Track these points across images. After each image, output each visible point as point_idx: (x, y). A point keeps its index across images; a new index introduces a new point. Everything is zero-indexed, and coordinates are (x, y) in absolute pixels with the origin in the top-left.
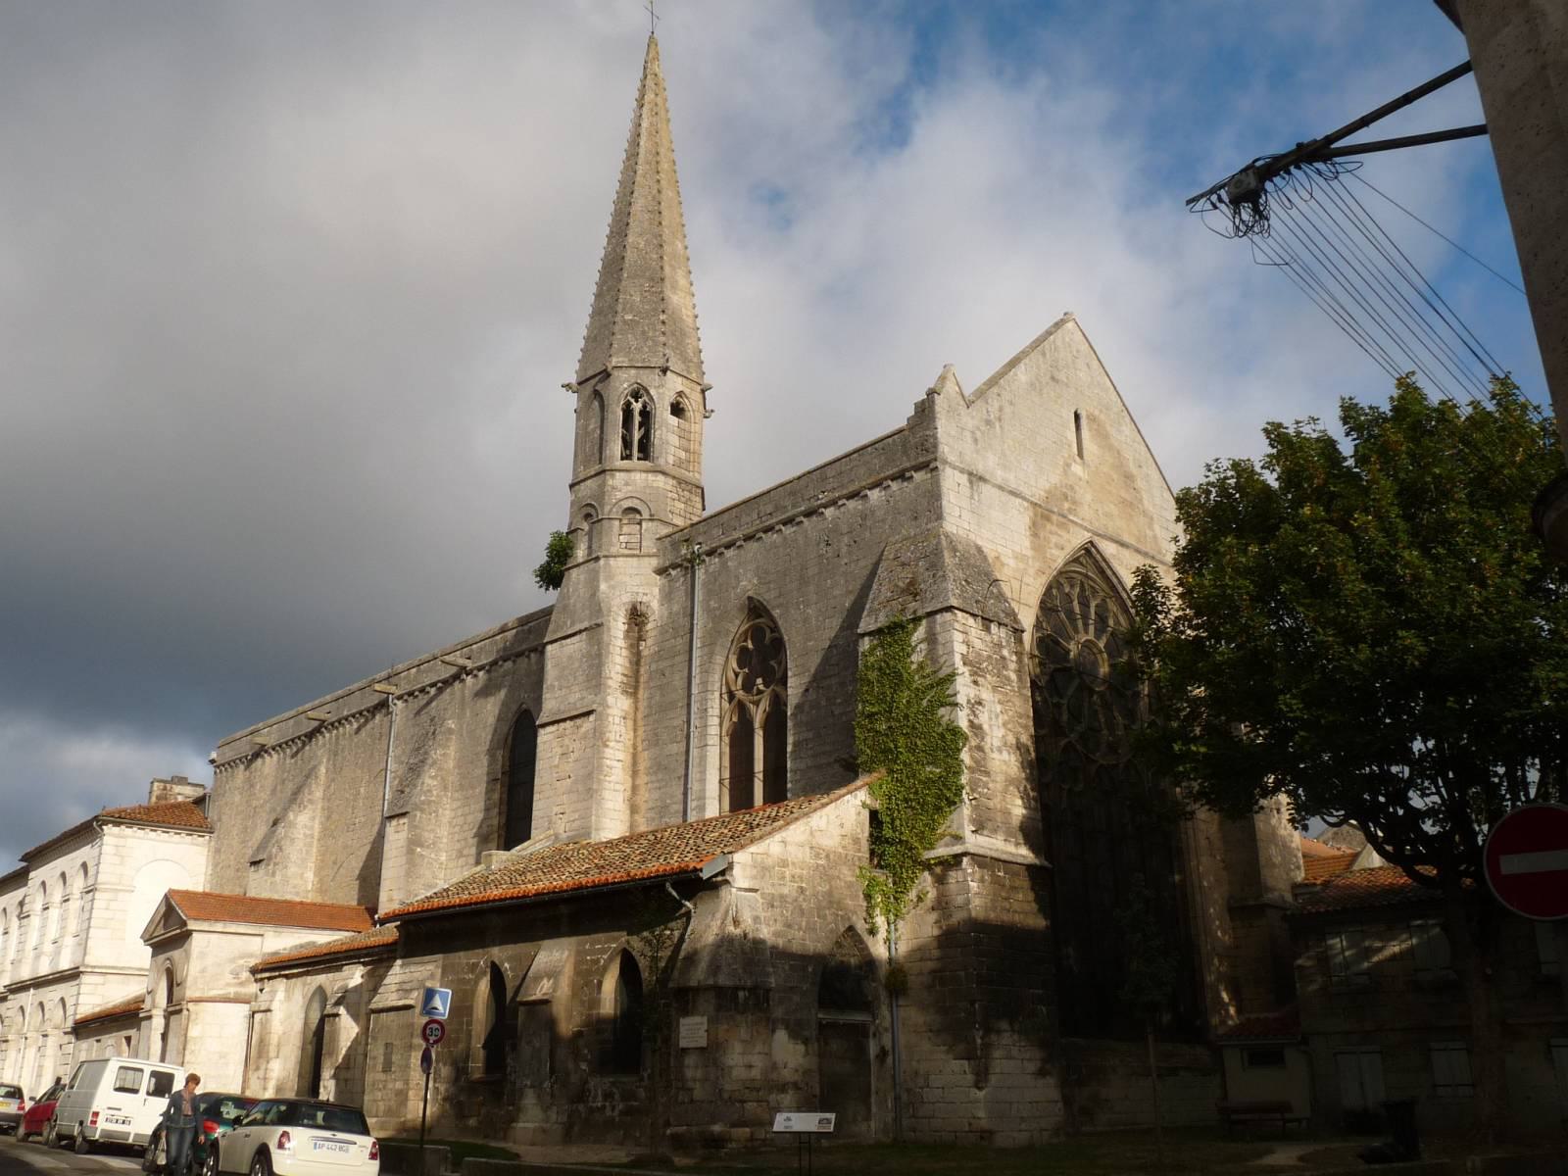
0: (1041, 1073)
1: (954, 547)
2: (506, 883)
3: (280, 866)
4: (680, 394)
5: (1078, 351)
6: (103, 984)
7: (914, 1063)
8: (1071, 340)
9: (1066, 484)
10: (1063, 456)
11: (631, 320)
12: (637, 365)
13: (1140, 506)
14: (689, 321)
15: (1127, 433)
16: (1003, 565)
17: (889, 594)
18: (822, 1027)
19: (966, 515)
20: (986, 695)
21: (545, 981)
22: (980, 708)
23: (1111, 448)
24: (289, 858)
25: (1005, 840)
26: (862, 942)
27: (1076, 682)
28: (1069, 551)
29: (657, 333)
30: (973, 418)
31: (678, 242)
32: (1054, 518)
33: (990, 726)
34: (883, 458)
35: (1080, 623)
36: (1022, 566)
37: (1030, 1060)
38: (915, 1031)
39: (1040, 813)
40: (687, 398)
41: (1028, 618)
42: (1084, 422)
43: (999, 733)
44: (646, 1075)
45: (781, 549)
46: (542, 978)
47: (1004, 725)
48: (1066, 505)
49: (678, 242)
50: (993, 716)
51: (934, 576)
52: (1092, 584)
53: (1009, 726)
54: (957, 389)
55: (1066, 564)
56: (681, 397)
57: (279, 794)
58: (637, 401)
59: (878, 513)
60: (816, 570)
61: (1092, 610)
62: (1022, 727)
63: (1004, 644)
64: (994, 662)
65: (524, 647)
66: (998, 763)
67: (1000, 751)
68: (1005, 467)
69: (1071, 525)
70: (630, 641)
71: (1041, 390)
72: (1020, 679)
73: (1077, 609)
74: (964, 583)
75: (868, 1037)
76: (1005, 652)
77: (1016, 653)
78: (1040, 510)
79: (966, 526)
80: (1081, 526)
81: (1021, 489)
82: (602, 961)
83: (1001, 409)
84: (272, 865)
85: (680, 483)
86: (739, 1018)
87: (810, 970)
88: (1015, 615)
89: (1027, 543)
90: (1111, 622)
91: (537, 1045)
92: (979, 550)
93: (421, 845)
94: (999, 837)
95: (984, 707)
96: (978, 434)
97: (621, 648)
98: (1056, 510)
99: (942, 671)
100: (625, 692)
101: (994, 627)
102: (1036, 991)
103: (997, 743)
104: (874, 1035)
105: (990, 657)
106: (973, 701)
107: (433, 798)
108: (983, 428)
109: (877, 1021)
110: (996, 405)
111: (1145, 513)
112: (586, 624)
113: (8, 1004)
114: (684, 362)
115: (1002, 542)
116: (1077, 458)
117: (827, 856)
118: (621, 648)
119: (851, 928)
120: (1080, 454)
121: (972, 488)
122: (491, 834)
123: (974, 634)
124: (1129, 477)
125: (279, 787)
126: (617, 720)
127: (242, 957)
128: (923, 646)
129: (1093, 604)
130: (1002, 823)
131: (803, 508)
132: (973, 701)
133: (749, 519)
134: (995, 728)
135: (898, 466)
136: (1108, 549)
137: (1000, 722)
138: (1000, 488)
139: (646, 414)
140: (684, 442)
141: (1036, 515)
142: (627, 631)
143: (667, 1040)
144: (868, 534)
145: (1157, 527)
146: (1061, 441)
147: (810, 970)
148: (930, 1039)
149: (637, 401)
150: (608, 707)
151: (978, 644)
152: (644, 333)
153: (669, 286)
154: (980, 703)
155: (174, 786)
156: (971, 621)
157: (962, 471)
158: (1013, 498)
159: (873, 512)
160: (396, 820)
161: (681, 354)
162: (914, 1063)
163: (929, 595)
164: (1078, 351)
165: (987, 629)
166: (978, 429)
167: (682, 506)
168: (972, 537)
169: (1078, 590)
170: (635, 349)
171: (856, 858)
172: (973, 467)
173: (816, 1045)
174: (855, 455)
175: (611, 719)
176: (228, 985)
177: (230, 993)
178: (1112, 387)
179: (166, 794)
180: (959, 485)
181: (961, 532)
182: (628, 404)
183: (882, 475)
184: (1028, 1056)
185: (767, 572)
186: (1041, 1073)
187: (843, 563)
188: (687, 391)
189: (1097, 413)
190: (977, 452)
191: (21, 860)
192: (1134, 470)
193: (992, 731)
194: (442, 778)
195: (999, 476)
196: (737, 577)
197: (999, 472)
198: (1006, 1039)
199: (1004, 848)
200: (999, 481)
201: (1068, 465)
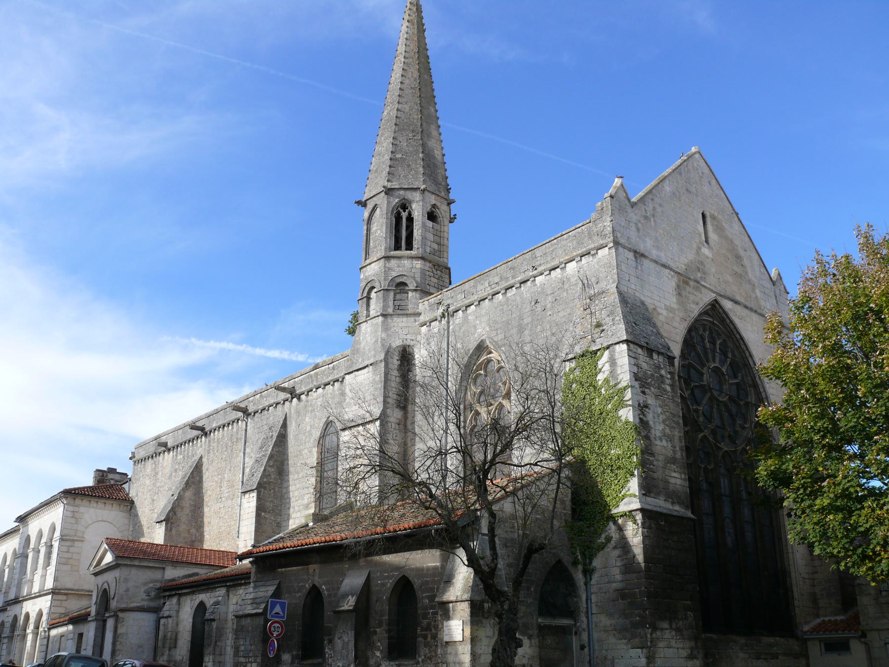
0: (691, 657)
1: (626, 300)
2: (321, 533)
3: (175, 525)
4: (434, 206)
5: (703, 173)
6: (66, 600)
7: (604, 651)
8: (698, 165)
9: (699, 261)
10: (696, 242)
11: (400, 158)
12: (404, 187)
13: (746, 277)
14: (439, 158)
15: (736, 228)
16: (659, 314)
17: (582, 333)
18: (541, 628)
19: (633, 280)
20: (651, 401)
21: (350, 597)
22: (647, 410)
23: (726, 238)
24: (180, 520)
25: (665, 500)
26: (567, 570)
27: (708, 395)
28: (701, 306)
29: (418, 166)
30: (635, 214)
31: (431, 107)
32: (692, 283)
33: (654, 423)
34: (574, 242)
35: (710, 357)
36: (671, 315)
37: (683, 648)
38: (604, 631)
39: (688, 482)
40: (438, 208)
41: (676, 350)
42: (708, 220)
43: (660, 427)
44: (420, 660)
45: (505, 306)
46: (348, 596)
47: (664, 422)
48: (699, 275)
49: (431, 107)
50: (656, 416)
51: (613, 320)
52: (717, 329)
53: (667, 423)
54: (624, 194)
55: (701, 314)
56: (435, 208)
57: (173, 478)
58: (404, 211)
59: (572, 280)
60: (530, 319)
61: (718, 347)
62: (675, 423)
63: (662, 366)
64: (655, 379)
65: (330, 378)
66: (659, 447)
67: (661, 440)
68: (658, 248)
69: (703, 290)
70: (402, 372)
71: (680, 197)
72: (673, 389)
73: (708, 345)
74: (634, 324)
75: (571, 634)
76: (663, 372)
77: (670, 372)
78: (682, 278)
79: (633, 287)
80: (709, 289)
81: (669, 263)
82: (389, 584)
83: (654, 209)
84: (170, 524)
85: (434, 266)
86: (484, 621)
87: (532, 589)
88: (669, 349)
89: (674, 300)
90: (730, 355)
91: (346, 639)
92: (643, 303)
93: (265, 512)
94: (661, 498)
95: (649, 409)
96: (640, 225)
97: (396, 377)
98: (692, 278)
99: (620, 385)
100: (398, 406)
101: (655, 356)
102: (686, 602)
103: (658, 434)
104: (576, 633)
105: (653, 375)
106: (642, 405)
107: (272, 480)
108: (643, 222)
109: (578, 624)
110: (651, 206)
111: (750, 282)
112: (372, 361)
113: (7, 614)
114: (436, 185)
115: (658, 298)
116: (705, 244)
117: (543, 513)
118: (396, 377)
119: (559, 562)
120: (707, 241)
121: (636, 261)
122: (310, 503)
123: (641, 359)
124: (738, 257)
125: (173, 474)
126: (393, 425)
127: (152, 582)
128: (607, 365)
129: (718, 342)
130: (663, 489)
131: (519, 278)
132: (642, 405)
133: (482, 287)
134: (657, 424)
135: (585, 247)
136: (727, 305)
137: (661, 419)
138: (656, 262)
139: (410, 219)
140: (436, 238)
141: (679, 281)
142: (400, 365)
143: (435, 637)
144: (565, 294)
145: (757, 291)
146: (695, 232)
147: (532, 589)
148: (614, 635)
149: (404, 211)
150: (388, 417)
151: (645, 366)
152: (409, 166)
153: (425, 136)
154: (646, 406)
155: (108, 474)
156: (640, 351)
157: (630, 250)
158: (664, 269)
159: (569, 279)
160: (248, 494)
161: (434, 180)
162: (604, 652)
163: (610, 333)
164: (703, 173)
165: (651, 357)
166: (639, 221)
167: (436, 281)
168: (637, 294)
169: (707, 333)
170: (403, 176)
171: (562, 514)
172: (637, 247)
173: (537, 640)
174: (555, 241)
175: (390, 424)
176: (143, 600)
177: (144, 605)
178: (725, 198)
179: (104, 479)
180: (628, 259)
181: (630, 291)
182: (399, 213)
183: (575, 254)
184: (681, 646)
185: (495, 322)
186: (691, 657)
187: (548, 315)
188: (438, 204)
189: (716, 214)
190: (639, 237)
191: (15, 522)
192: (742, 253)
193: (655, 427)
194: (277, 467)
195: (654, 253)
196: (475, 327)
197: (654, 251)
198: (667, 634)
199: (664, 505)
200: (654, 257)
201: (699, 248)
